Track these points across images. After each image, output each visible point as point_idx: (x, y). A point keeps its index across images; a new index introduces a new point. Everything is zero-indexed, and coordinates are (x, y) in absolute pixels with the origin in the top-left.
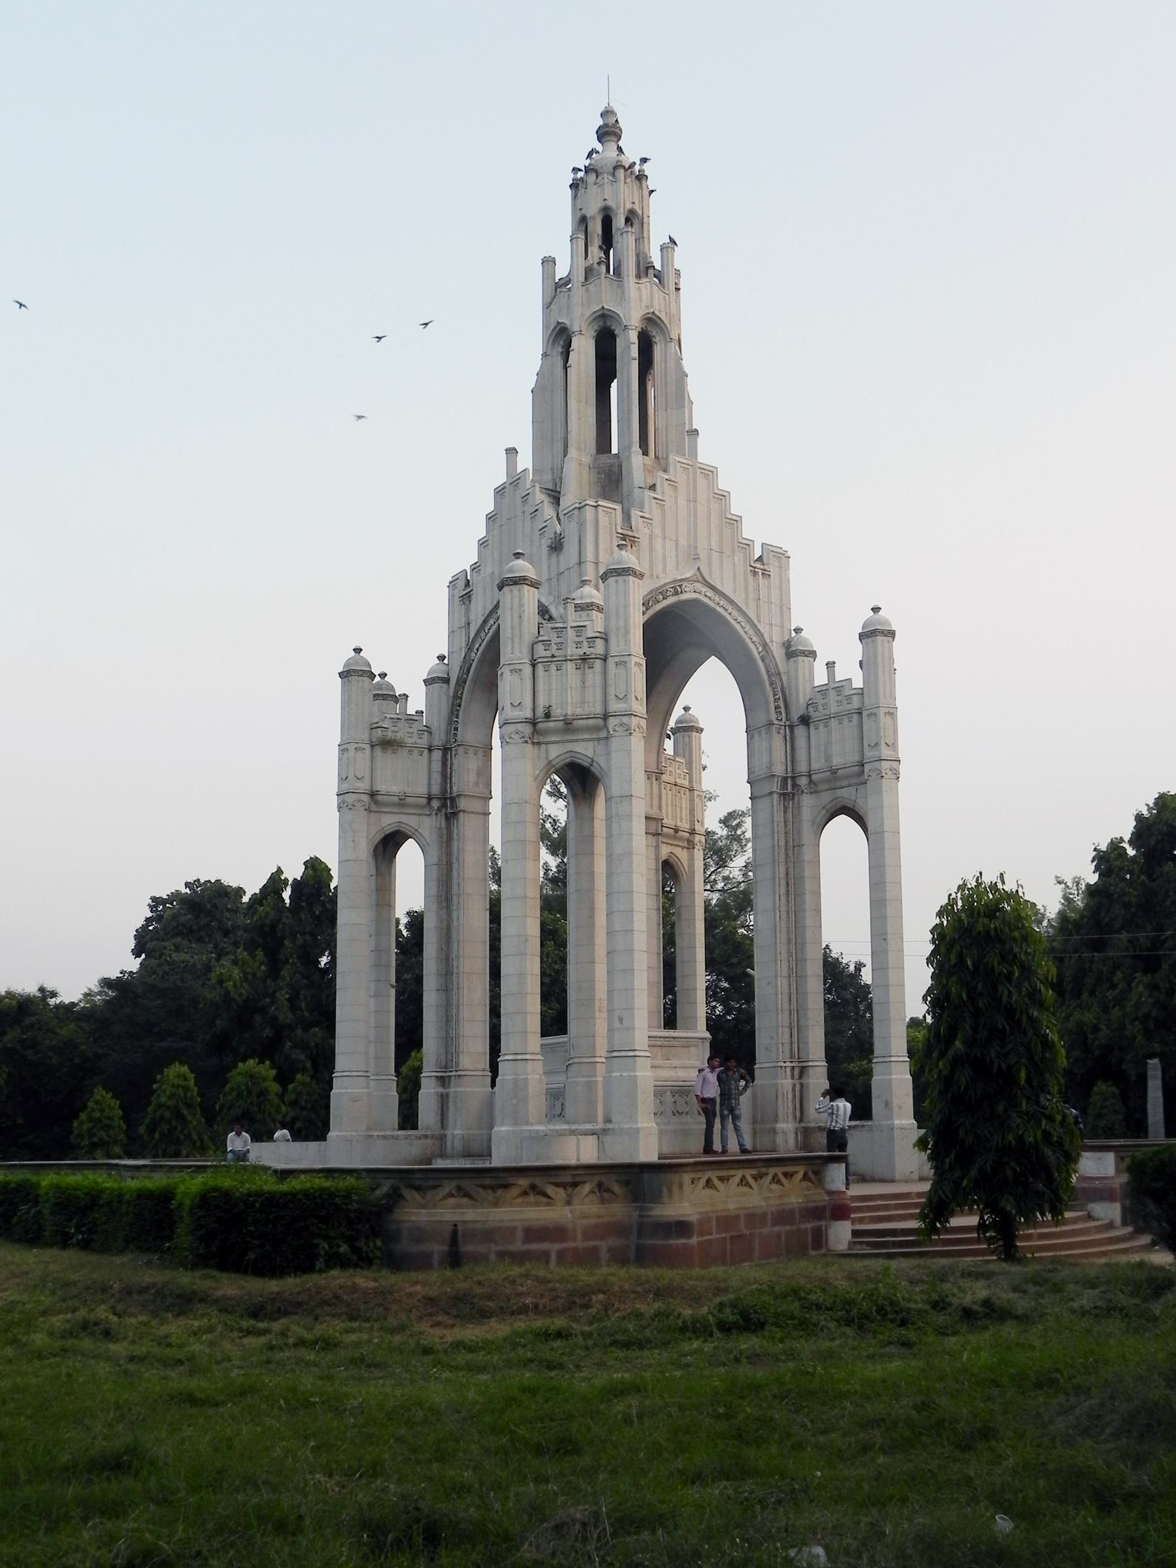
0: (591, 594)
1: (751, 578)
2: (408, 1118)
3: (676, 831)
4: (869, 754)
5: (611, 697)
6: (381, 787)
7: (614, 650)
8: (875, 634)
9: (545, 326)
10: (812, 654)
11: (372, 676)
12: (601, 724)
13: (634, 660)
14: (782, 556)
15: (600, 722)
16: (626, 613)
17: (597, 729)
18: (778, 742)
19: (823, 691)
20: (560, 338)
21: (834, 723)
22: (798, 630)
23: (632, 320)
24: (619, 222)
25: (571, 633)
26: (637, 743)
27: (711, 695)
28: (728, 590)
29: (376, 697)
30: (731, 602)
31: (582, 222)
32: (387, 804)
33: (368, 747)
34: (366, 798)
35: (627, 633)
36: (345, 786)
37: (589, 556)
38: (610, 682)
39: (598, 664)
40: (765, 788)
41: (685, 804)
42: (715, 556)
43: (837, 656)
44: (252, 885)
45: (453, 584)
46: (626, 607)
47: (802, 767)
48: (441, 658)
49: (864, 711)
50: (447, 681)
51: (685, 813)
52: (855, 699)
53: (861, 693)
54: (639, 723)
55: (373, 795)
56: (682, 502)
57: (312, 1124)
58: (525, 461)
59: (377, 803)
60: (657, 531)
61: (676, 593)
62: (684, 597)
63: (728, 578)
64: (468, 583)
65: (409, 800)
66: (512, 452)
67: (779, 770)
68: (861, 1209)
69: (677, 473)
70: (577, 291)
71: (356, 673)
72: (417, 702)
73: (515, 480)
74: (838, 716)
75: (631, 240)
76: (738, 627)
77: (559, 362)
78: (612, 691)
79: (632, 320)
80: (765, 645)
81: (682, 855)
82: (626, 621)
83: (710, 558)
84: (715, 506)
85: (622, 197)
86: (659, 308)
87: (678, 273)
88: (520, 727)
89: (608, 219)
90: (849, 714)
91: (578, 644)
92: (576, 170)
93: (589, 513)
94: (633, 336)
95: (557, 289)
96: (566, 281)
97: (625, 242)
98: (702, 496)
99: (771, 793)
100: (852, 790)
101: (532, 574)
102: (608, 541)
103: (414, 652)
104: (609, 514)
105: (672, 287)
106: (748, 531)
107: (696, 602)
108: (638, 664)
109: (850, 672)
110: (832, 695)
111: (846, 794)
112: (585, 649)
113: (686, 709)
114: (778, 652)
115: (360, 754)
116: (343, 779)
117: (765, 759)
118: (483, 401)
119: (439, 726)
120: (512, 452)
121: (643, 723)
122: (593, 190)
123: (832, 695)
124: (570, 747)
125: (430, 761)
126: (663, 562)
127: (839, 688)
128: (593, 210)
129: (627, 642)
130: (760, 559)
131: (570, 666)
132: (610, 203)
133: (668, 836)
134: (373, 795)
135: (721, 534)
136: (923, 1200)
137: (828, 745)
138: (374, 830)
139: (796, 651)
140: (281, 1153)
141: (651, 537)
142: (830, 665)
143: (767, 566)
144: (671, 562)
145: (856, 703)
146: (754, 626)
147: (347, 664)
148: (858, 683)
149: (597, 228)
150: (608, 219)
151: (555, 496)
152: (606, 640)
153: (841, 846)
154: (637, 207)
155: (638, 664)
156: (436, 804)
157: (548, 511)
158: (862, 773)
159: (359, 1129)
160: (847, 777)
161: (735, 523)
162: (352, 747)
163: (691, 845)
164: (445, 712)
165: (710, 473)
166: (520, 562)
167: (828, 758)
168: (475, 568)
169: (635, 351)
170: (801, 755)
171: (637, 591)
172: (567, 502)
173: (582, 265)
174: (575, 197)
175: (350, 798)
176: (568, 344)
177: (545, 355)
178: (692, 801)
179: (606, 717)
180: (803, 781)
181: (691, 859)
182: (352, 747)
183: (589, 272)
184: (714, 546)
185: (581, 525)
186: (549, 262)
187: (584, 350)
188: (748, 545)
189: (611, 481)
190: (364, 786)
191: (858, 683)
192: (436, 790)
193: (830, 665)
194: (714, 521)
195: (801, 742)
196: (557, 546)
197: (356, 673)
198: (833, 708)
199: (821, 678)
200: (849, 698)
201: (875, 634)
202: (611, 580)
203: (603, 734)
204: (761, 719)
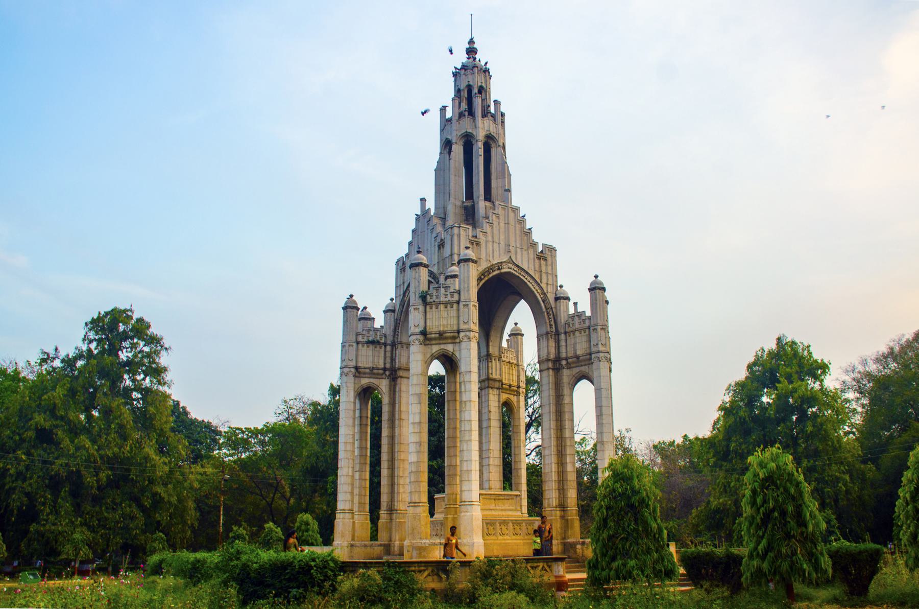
0: (455, 269)
1: (537, 261)
2: (374, 537)
3: (510, 386)
4: (594, 349)
5: (461, 322)
6: (360, 365)
7: (462, 298)
8: (596, 289)
9: (441, 140)
10: (568, 299)
11: (358, 309)
12: (455, 337)
13: (472, 303)
14: (552, 250)
15: (456, 334)
16: (468, 280)
17: (454, 338)
18: (552, 344)
19: (572, 317)
20: (447, 145)
21: (577, 333)
22: (561, 286)
23: (481, 135)
24: (475, 90)
25: (442, 290)
26: (474, 345)
27: (522, 316)
28: (525, 267)
29: (360, 319)
30: (527, 273)
31: (458, 91)
32: (365, 373)
33: (355, 345)
34: (353, 370)
35: (468, 290)
36: (344, 364)
37: (456, 251)
38: (461, 314)
39: (455, 306)
40: (545, 366)
41: (515, 373)
42: (519, 250)
43: (580, 301)
44: (679, 440)
45: (398, 261)
46: (468, 277)
47: (563, 355)
48: (392, 299)
49: (593, 326)
50: (393, 311)
51: (515, 378)
52: (587, 321)
53: (589, 318)
54: (475, 335)
55: (357, 368)
56: (502, 225)
57: (327, 537)
58: (431, 205)
59: (359, 373)
60: (490, 238)
61: (499, 269)
62: (503, 271)
63: (526, 262)
64: (404, 263)
65: (375, 371)
66: (423, 200)
67: (552, 356)
68: (573, 586)
69: (499, 210)
70: (455, 124)
71: (350, 307)
72: (379, 322)
73: (425, 212)
74: (580, 330)
75: (480, 100)
76: (530, 285)
77: (447, 155)
78: (461, 319)
79: (481, 135)
80: (545, 294)
81: (514, 399)
82: (468, 284)
83: (516, 252)
84: (518, 226)
85: (477, 80)
86: (493, 130)
87: (503, 115)
88: (418, 337)
89: (472, 90)
90: (584, 330)
91: (446, 296)
92: (456, 68)
93: (456, 230)
94: (480, 145)
95: (446, 123)
96: (450, 120)
97: (478, 102)
98: (512, 222)
99: (548, 369)
100: (586, 367)
101: (425, 261)
102: (464, 242)
103: (377, 301)
104: (465, 233)
105: (500, 121)
106: (535, 237)
107: (509, 273)
108: (474, 306)
109: (585, 307)
110: (576, 319)
111: (584, 369)
112: (449, 298)
113: (516, 324)
114: (551, 297)
115: (351, 348)
116: (343, 360)
117: (546, 351)
118: (411, 176)
119: (389, 332)
120: (423, 200)
121: (477, 335)
122: (463, 77)
123: (576, 319)
124: (442, 346)
125: (385, 352)
126: (494, 251)
127: (579, 315)
128: (463, 86)
129: (469, 294)
130: (542, 252)
131: (442, 307)
132: (471, 83)
133: (506, 389)
134: (357, 368)
135: (522, 239)
136: (584, 575)
137: (575, 344)
138: (357, 387)
139: (561, 298)
140: (321, 551)
141: (487, 242)
142: (575, 304)
143: (546, 255)
144: (496, 254)
145: (587, 324)
146: (538, 285)
147: (346, 303)
148: (588, 313)
149: (465, 94)
150: (472, 90)
151: (444, 219)
152: (459, 294)
153: (583, 396)
154: (484, 85)
155: (474, 306)
156: (387, 373)
157: (439, 229)
158: (590, 359)
159: (348, 538)
160: (584, 360)
161: (529, 232)
162: (347, 344)
163: (518, 394)
164: (392, 327)
165: (516, 210)
166: (420, 255)
167: (575, 350)
168: (407, 255)
169: (481, 152)
170: (563, 350)
171: (473, 272)
172: (449, 223)
173: (457, 111)
174: (455, 81)
175: (346, 370)
176: (450, 149)
177: (441, 153)
178: (518, 371)
179: (458, 332)
180: (564, 362)
181: (518, 401)
182: (347, 344)
183: (461, 115)
184: (518, 245)
185: (452, 236)
186: (443, 109)
187: (458, 150)
188: (534, 245)
189: (470, 215)
190: (353, 364)
191: (588, 313)
192: (388, 366)
193: (575, 304)
194: (518, 233)
195: (563, 343)
196: (441, 245)
197: (350, 307)
198: (577, 326)
199: (572, 311)
200: (584, 321)
201: (596, 289)
202: (462, 264)
203: (458, 340)
204: (544, 331)
